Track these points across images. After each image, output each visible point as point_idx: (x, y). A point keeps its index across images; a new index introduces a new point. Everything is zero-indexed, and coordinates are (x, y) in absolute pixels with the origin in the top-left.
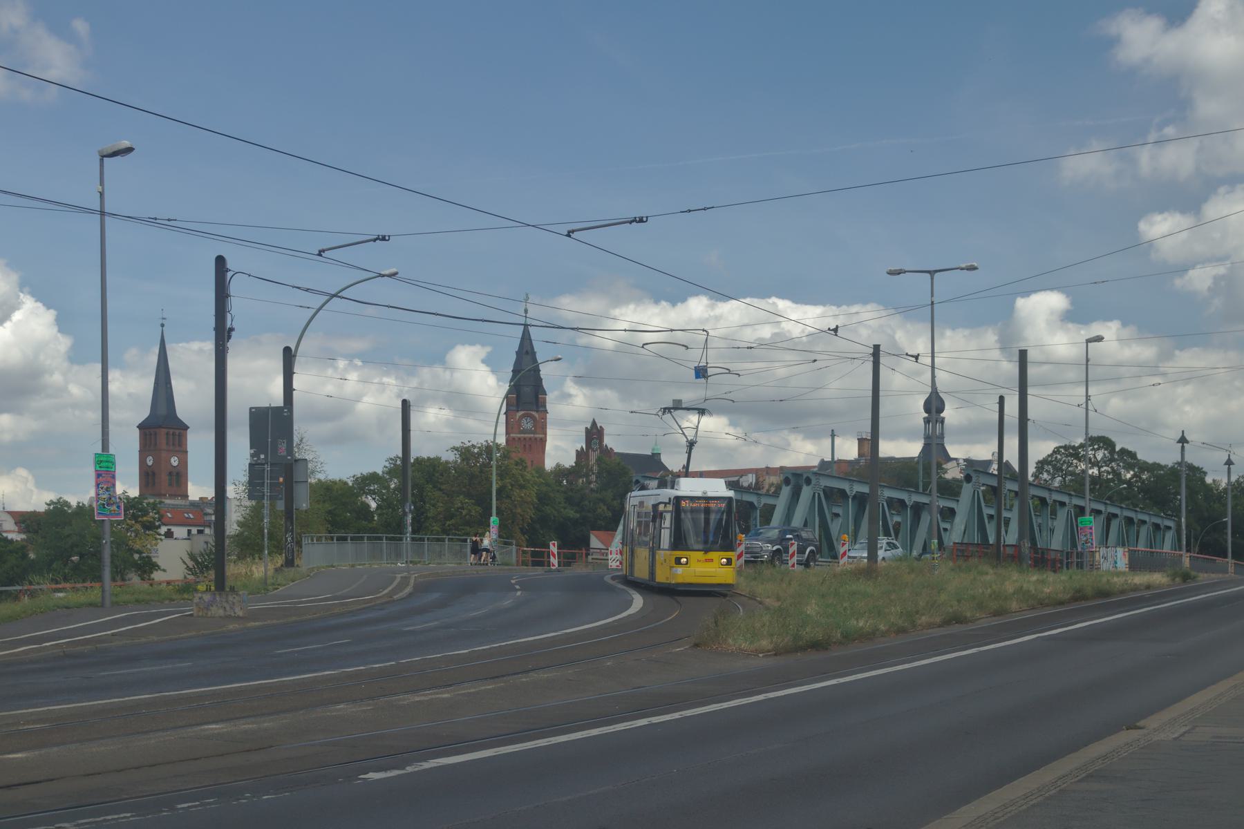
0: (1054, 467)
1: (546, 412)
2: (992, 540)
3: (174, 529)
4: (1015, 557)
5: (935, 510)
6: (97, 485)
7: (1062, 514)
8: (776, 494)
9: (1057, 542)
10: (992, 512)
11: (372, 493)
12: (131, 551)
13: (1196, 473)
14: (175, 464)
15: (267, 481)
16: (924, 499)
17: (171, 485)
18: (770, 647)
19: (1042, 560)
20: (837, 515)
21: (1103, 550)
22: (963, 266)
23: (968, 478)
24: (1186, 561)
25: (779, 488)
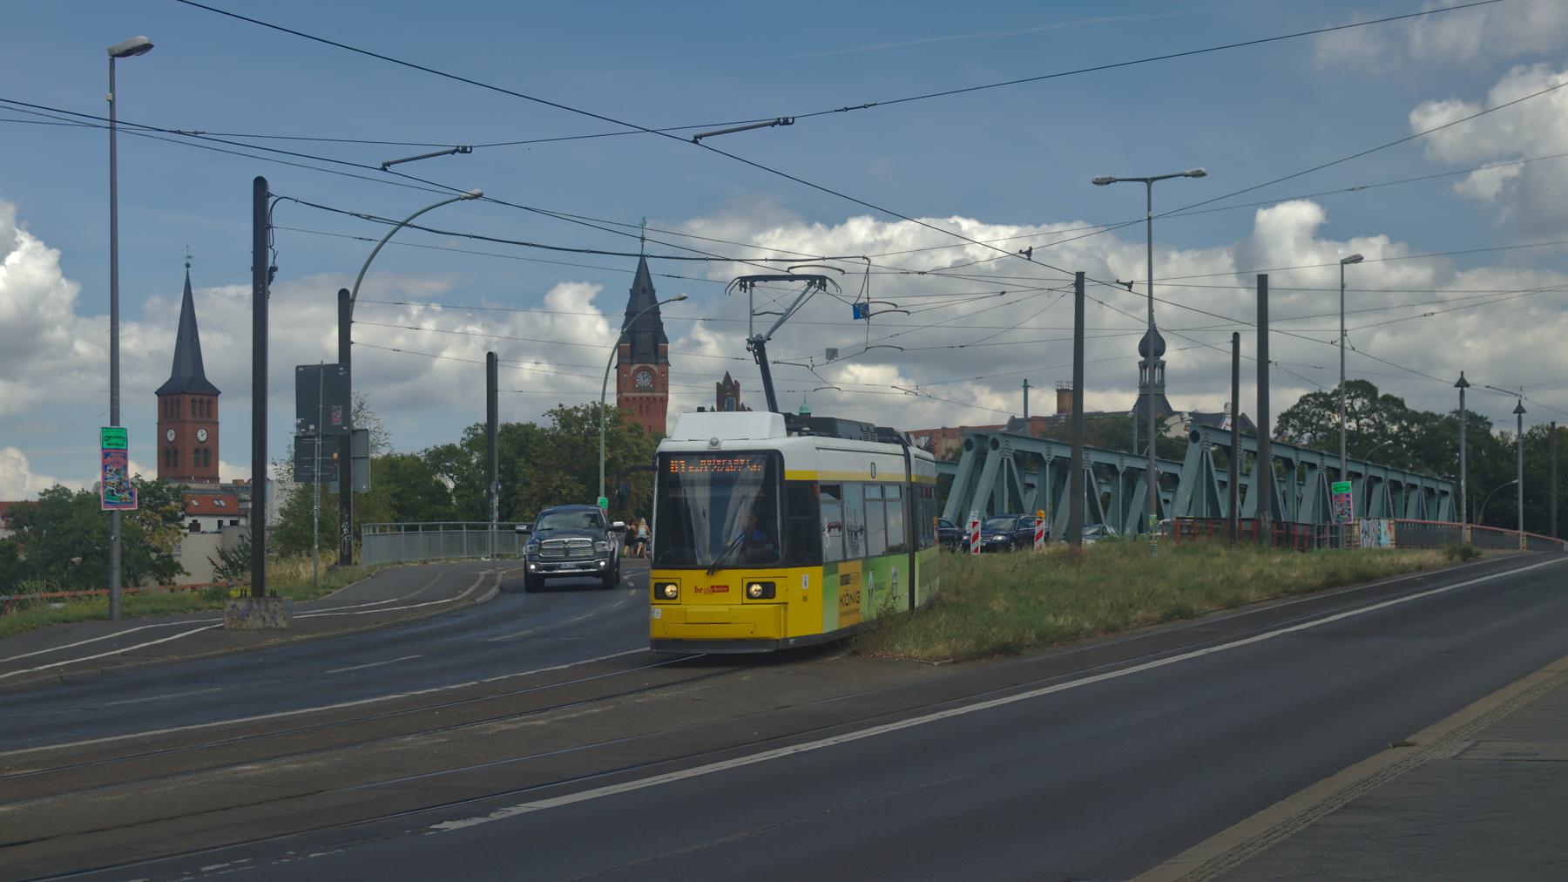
0: (1301, 420)
1: (667, 364)
3: (200, 520)
4: (1253, 534)
6: (105, 467)
7: (1312, 478)
8: (955, 461)
10: (1224, 478)
11: (449, 470)
13: (1478, 424)
15: (318, 458)
16: (1140, 464)
17: (197, 464)
18: (948, 653)
19: (1287, 537)
20: (1031, 486)
21: (1363, 523)
23: (1195, 437)
24: (1467, 534)
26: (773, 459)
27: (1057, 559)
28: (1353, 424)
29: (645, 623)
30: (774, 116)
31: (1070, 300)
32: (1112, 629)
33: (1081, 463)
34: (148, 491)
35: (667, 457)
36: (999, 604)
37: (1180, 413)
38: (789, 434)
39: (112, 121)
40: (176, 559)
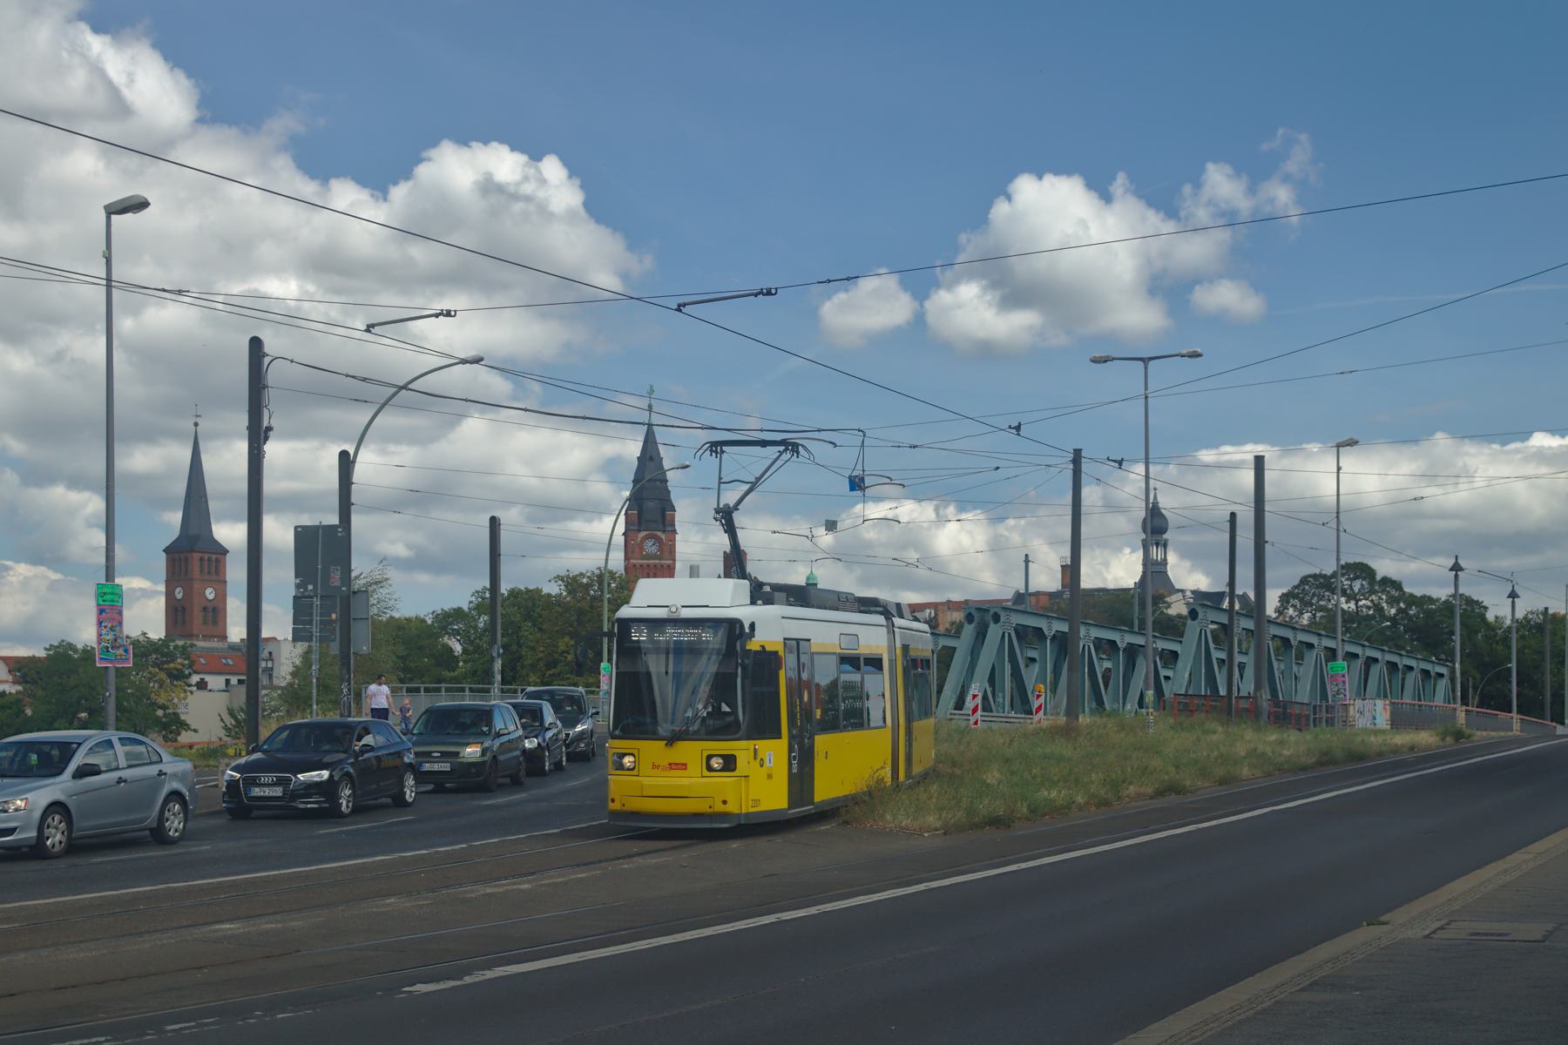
0: (1302, 600)
1: (675, 532)
2: (1223, 692)
3: (208, 678)
4: (1251, 713)
5: (1150, 653)
6: (100, 623)
7: (1310, 657)
8: (957, 635)
9: (1304, 693)
10: (1223, 655)
11: (456, 633)
12: (155, 705)
13: (1473, 610)
14: (211, 597)
15: (316, 618)
16: (1140, 640)
17: (205, 623)
18: (938, 824)
19: (1283, 715)
20: (1033, 660)
21: (1359, 703)
22: (1184, 352)
23: (1193, 614)
24: (1461, 717)
25: (960, 627)
26: (734, 631)
27: (1054, 732)
28: (1352, 605)
29: (604, 799)
30: (756, 287)
31: (1069, 473)
32: (1105, 803)
33: (1061, 639)
34: (144, 650)
35: (626, 624)
36: (993, 776)
37: (1182, 591)
38: (753, 603)
39: (109, 279)
40: (183, 717)
